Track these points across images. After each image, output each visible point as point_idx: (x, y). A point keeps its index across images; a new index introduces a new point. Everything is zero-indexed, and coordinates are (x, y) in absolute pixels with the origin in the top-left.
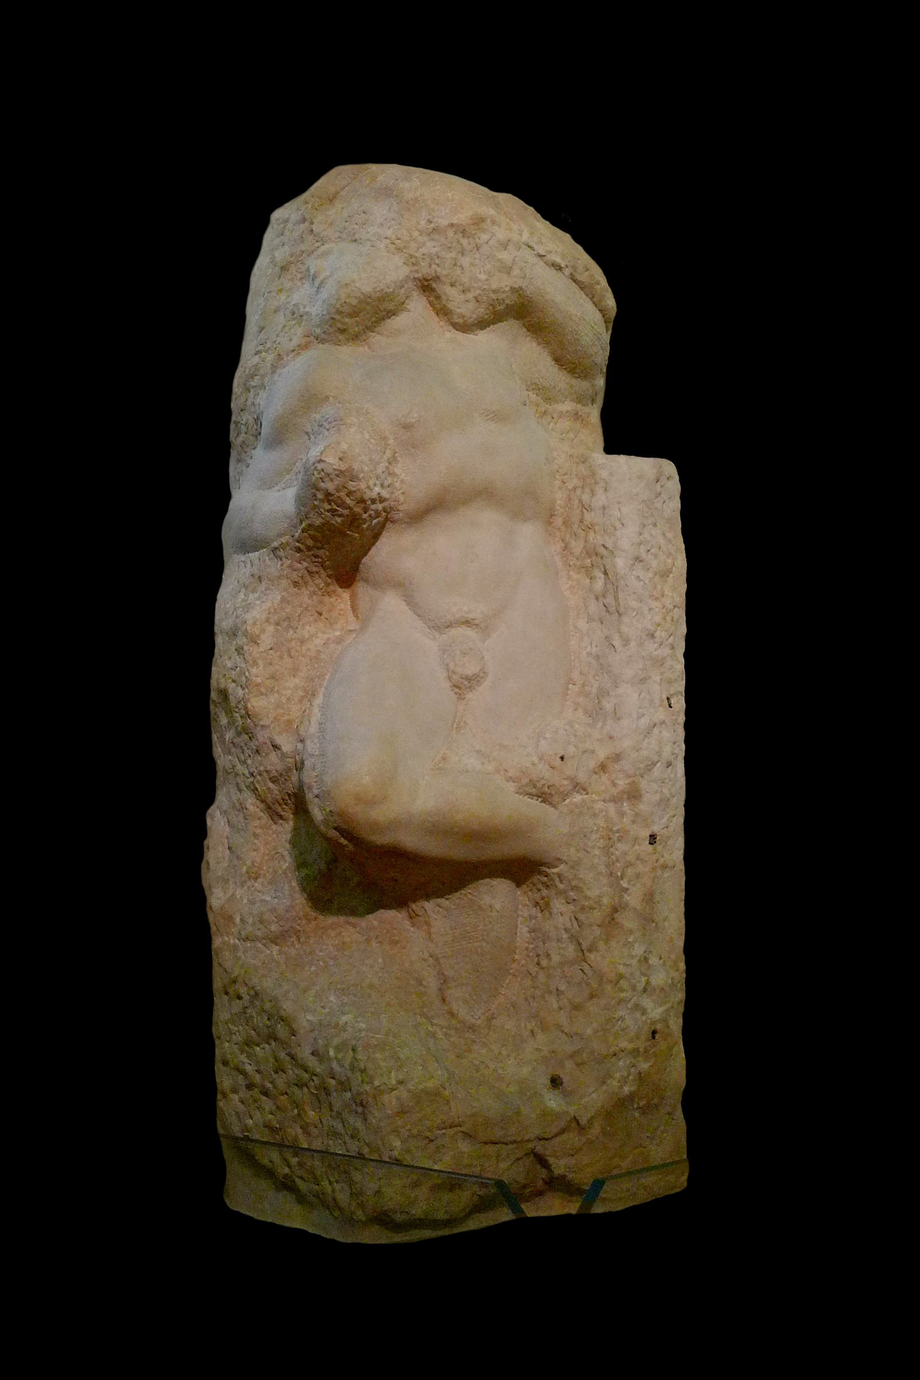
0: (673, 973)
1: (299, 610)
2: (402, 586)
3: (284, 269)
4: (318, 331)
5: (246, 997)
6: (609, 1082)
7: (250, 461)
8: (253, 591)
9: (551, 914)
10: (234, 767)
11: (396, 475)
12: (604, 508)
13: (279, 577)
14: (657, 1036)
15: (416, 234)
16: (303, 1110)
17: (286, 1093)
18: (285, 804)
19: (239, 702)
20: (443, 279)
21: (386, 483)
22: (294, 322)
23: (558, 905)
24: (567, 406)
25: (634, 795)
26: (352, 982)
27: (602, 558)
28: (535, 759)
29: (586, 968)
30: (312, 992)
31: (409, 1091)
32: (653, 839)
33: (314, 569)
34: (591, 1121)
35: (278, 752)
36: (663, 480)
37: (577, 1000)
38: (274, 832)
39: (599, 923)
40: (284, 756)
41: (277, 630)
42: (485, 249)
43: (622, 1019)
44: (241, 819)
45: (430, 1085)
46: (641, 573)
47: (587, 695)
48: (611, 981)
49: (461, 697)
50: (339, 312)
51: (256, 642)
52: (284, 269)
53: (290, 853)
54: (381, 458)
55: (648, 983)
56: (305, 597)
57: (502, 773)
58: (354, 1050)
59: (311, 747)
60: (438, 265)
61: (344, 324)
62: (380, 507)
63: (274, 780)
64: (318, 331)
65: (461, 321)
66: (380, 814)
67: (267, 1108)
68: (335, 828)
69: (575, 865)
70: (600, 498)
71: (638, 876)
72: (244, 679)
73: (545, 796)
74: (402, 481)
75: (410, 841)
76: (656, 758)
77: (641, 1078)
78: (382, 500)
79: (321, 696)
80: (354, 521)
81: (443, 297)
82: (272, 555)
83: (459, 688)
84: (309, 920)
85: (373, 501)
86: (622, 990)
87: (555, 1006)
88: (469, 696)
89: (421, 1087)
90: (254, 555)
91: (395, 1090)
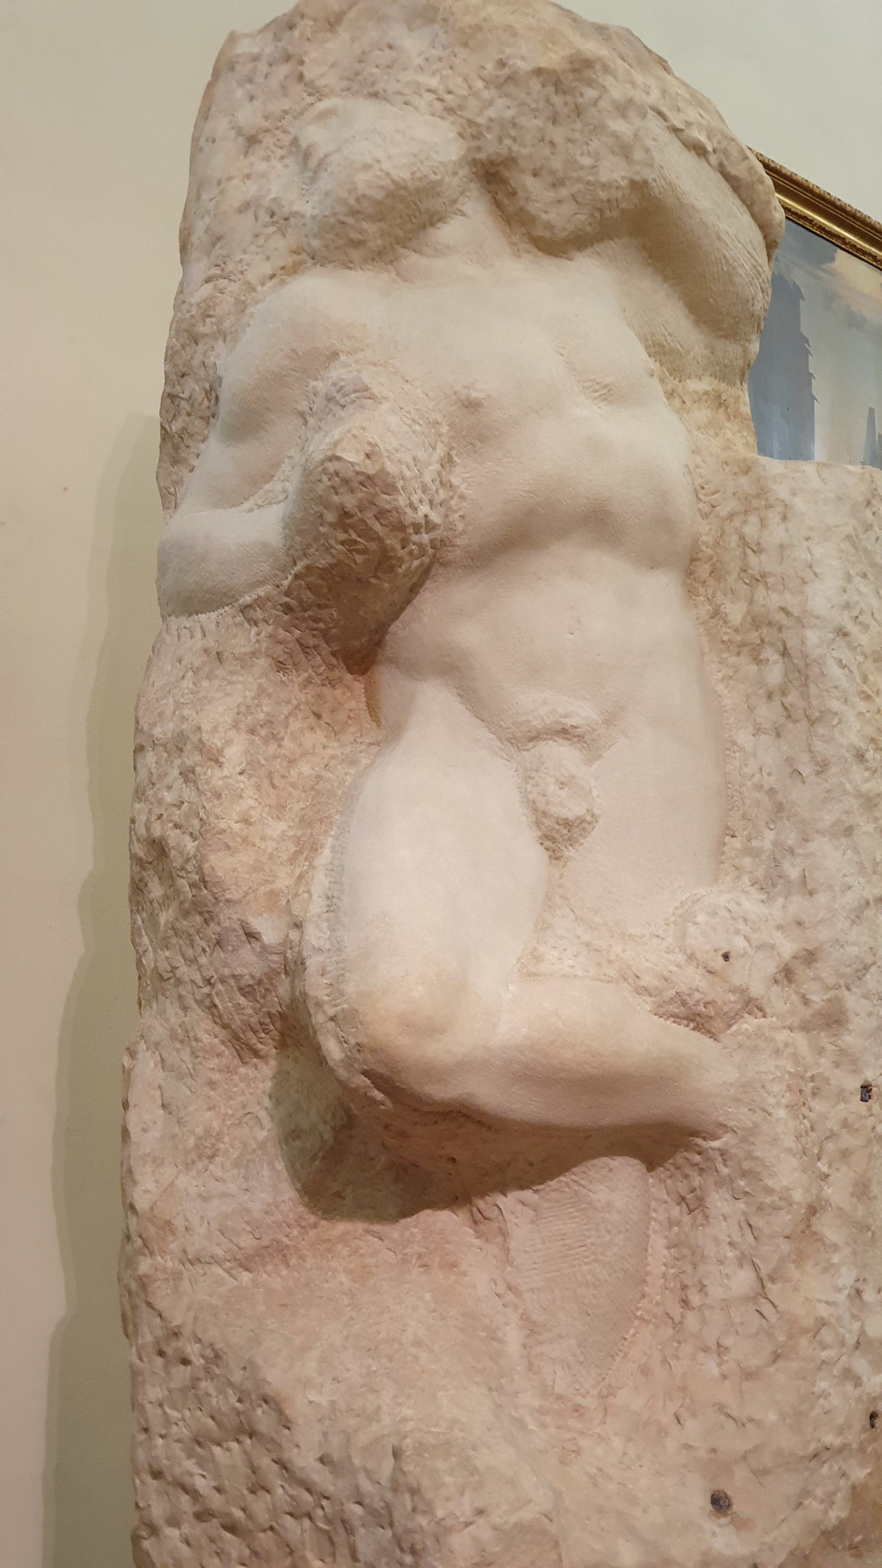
1: (286, 710)
2: (454, 669)
4: (316, 243)
5: (198, 1361)
6: (807, 1502)
7: (195, 462)
9: (706, 1217)
10: (174, 969)
11: (451, 486)
14: (878, 1422)
15: (480, 84)
16: (303, 1558)
17: (272, 1528)
18: (264, 1030)
19: (188, 860)
20: (522, 162)
21: (437, 500)
22: (272, 229)
23: (719, 1202)
24: (705, 385)
25: (833, 1019)
26: (383, 1335)
27: (780, 629)
28: (680, 958)
29: (766, 1308)
30: (315, 1354)
31: (495, 1528)
32: (866, 1091)
33: (311, 642)
35: (257, 945)
37: (754, 1362)
38: (243, 1079)
39: (787, 1232)
41: (252, 742)
43: (824, 1394)
44: (186, 1055)
45: (527, 1515)
46: (847, 656)
47: (755, 853)
48: (805, 1331)
49: (555, 856)
50: (353, 213)
51: (217, 761)
52: (252, 140)
54: (430, 456)
55: (863, 1332)
59: (315, 935)
60: (514, 140)
62: (425, 538)
63: (247, 991)
64: (316, 243)
65: (547, 234)
66: (439, 1050)
67: (234, 1554)
68: (365, 1073)
69: (749, 1135)
70: (777, 533)
71: (845, 1154)
72: (196, 822)
73: (698, 1019)
74: (462, 497)
75: (488, 1094)
76: (869, 959)
78: (430, 526)
79: (327, 852)
80: (385, 562)
81: (521, 194)
82: (240, 618)
83: (554, 840)
84: (303, 1227)
85: (417, 528)
86: (824, 1347)
88: (570, 852)
89: (514, 1519)
90: (208, 619)
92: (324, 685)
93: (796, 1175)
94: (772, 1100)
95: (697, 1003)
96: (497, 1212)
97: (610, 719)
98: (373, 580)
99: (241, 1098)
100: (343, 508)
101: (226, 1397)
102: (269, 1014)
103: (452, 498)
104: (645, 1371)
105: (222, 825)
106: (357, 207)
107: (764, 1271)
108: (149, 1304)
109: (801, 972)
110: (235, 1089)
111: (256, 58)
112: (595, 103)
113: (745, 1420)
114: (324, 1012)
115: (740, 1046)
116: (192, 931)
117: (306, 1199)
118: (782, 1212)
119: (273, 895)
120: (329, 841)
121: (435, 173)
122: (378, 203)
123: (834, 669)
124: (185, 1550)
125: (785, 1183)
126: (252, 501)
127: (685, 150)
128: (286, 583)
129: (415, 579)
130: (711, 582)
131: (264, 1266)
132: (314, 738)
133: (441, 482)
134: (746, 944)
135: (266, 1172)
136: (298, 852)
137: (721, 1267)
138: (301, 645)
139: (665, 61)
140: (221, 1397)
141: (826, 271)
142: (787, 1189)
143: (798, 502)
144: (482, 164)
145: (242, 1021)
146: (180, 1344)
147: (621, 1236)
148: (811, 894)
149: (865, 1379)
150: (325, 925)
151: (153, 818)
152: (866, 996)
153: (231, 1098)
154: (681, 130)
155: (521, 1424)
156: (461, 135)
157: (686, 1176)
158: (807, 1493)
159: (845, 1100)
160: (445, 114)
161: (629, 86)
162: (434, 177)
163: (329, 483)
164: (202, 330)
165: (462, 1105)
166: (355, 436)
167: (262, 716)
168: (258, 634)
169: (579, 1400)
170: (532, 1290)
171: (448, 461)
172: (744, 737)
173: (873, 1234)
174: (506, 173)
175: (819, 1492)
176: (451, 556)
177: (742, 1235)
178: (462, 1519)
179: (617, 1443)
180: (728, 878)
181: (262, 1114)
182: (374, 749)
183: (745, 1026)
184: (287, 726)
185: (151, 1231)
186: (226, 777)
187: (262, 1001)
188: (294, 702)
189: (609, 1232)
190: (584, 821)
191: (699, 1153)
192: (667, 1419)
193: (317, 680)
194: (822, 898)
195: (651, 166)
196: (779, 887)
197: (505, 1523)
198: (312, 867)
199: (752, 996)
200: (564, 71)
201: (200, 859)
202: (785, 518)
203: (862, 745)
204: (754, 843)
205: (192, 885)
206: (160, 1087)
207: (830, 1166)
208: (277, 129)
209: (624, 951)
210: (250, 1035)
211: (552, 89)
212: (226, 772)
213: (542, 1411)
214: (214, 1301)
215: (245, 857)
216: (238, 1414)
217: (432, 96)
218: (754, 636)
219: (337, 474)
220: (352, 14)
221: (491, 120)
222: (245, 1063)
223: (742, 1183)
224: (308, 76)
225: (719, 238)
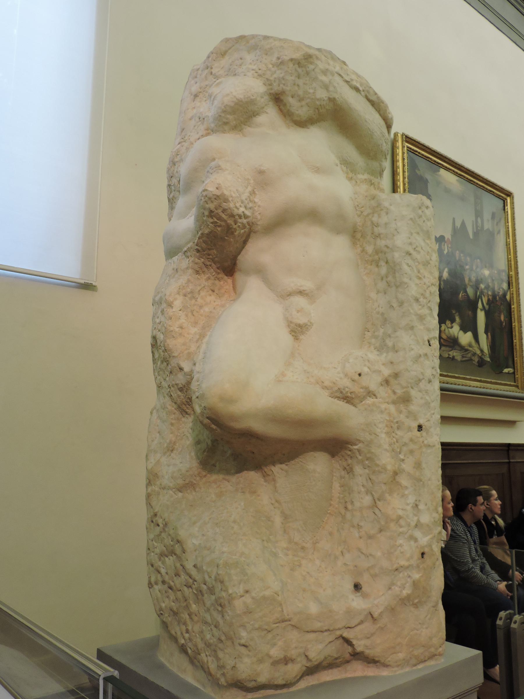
0: (435, 515)
1: (199, 288)
2: (260, 271)
3: (196, 96)
4: (213, 125)
6: (393, 588)
9: (354, 475)
12: (386, 224)
14: (425, 556)
15: (271, 66)
16: (189, 603)
17: (180, 590)
22: (200, 123)
23: (358, 469)
24: (366, 176)
25: (406, 399)
27: (385, 253)
28: (342, 375)
29: (377, 511)
31: (253, 598)
33: (208, 263)
34: (381, 614)
35: (183, 373)
36: (424, 208)
37: (372, 532)
43: (401, 545)
45: (267, 593)
46: (411, 262)
47: (376, 337)
48: (393, 520)
49: (296, 338)
52: (196, 96)
55: (418, 521)
56: (203, 280)
62: (245, 221)
66: (236, 409)
68: (207, 418)
70: (384, 219)
71: (411, 452)
73: (347, 398)
74: (259, 206)
75: (258, 426)
76: (421, 377)
77: (415, 584)
78: (246, 217)
80: (229, 230)
82: (184, 256)
84: (201, 477)
85: (240, 217)
86: (401, 527)
87: (357, 535)
88: (302, 337)
91: (243, 596)
94: (379, 430)
96: (271, 472)
98: (226, 238)
103: (255, 207)
104: (331, 534)
105: (172, 329)
107: (376, 496)
109: (392, 381)
115: (366, 409)
123: (405, 267)
124: (159, 595)
125: (384, 462)
128: (196, 241)
129: (244, 238)
130: (361, 239)
132: (211, 298)
133: (250, 200)
134: (369, 370)
138: (205, 265)
143: (392, 208)
148: (397, 352)
149: (419, 539)
152: (420, 391)
155: (275, 555)
156: (264, 84)
158: (393, 584)
159: (411, 431)
162: (252, 97)
164: (176, 160)
167: (189, 290)
169: (304, 544)
171: (253, 193)
172: (373, 295)
173: (423, 483)
174: (282, 98)
175: (399, 583)
178: (239, 594)
179: (318, 562)
181: (189, 435)
183: (368, 402)
188: (203, 285)
190: (307, 325)
191: (350, 451)
193: (213, 278)
198: (202, 343)
201: (165, 341)
202: (387, 213)
203: (418, 296)
204: (376, 334)
205: (163, 351)
210: (184, 406)
211: (297, 66)
212: (174, 310)
213: (287, 549)
215: (180, 340)
218: (376, 257)
221: (275, 78)
223: (367, 462)
225: (366, 121)
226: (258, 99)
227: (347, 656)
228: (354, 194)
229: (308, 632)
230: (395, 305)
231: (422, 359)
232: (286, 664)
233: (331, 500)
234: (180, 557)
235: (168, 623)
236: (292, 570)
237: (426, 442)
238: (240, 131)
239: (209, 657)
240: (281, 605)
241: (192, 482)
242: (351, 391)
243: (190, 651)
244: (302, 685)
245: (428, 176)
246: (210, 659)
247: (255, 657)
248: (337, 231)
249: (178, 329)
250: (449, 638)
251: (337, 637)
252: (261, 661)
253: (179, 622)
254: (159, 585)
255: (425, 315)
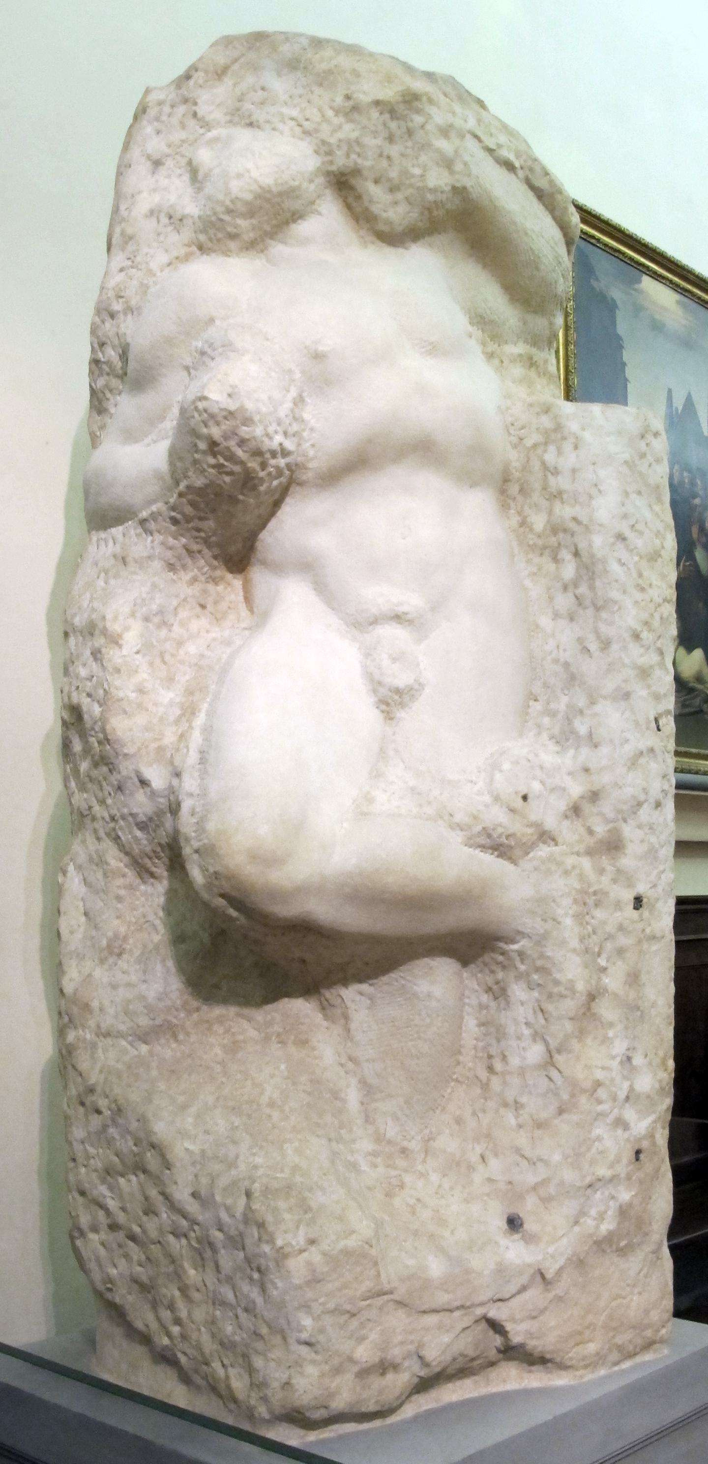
1: (175, 602)
2: (308, 567)
6: (582, 1221)
8: (116, 577)
9: (508, 1003)
10: (90, 808)
11: (303, 421)
12: (574, 471)
13: (150, 558)
14: (642, 1156)
15: (330, 113)
17: (159, 1242)
18: (156, 857)
19: (95, 723)
20: (365, 173)
23: (518, 991)
24: (520, 348)
25: (613, 845)
26: (246, 1097)
27: (572, 535)
28: (487, 799)
29: (554, 1074)
30: (192, 1110)
31: (324, 1254)
32: (638, 902)
33: (195, 547)
35: (148, 790)
36: (649, 437)
37: (543, 1115)
38: (145, 894)
39: (571, 1014)
40: (153, 794)
42: (420, 135)
43: (599, 1139)
44: (100, 875)
45: (351, 1242)
46: (624, 555)
47: (553, 714)
48: (584, 1091)
49: (389, 716)
50: (229, 211)
51: (117, 643)
52: (157, 163)
53: (164, 924)
55: (631, 1089)
57: (446, 818)
58: (248, 1194)
59: (189, 784)
60: (359, 155)
61: (236, 226)
62: (282, 462)
63: (142, 826)
65: (386, 229)
66: (284, 877)
68: (223, 896)
69: (542, 939)
70: (570, 459)
71: (620, 952)
72: (101, 692)
73: (501, 847)
75: (323, 911)
76: (642, 797)
78: (285, 453)
80: (248, 481)
81: (365, 197)
82: (140, 530)
83: (388, 704)
85: (274, 454)
86: (600, 1102)
88: (401, 714)
90: (117, 531)
91: (304, 1251)
92: (207, 582)
93: (579, 970)
95: (500, 836)
96: (340, 1000)
97: (434, 608)
98: (241, 497)
99: (141, 910)
100: (211, 438)
101: (126, 1141)
102: (160, 844)
103: (304, 430)
104: (459, 1121)
105: (121, 694)
106: (232, 207)
107: (553, 1044)
108: (74, 1067)
109: (587, 808)
110: (137, 903)
111: (160, 103)
112: (422, 127)
113: (535, 1160)
114: (191, 846)
115: (536, 869)
116: (101, 778)
117: (190, 989)
118: (569, 1000)
119: (160, 750)
120: (205, 706)
121: (294, 180)
122: (246, 203)
123: (614, 567)
124: (102, 1252)
125: (570, 976)
126: (150, 437)
127: (498, 166)
128: (172, 500)
129: (276, 496)
130: (520, 498)
131: (158, 1040)
133: (294, 417)
135: (159, 967)
136: (183, 715)
137: (519, 1042)
138: (187, 550)
139: (482, 101)
140: (123, 1141)
141: (635, 290)
142: (571, 981)
143: (587, 436)
144: (334, 175)
145: (140, 850)
146: (94, 1098)
147: (440, 1019)
148: (596, 746)
149: (632, 1125)
150: (196, 774)
151: (73, 688)
152: (640, 827)
153: (135, 909)
154: (494, 150)
155: (354, 1167)
157: (492, 972)
158: (582, 1213)
159: (621, 910)
160: (303, 136)
161: (450, 115)
163: (199, 419)
165: (304, 921)
166: (219, 381)
167: (154, 607)
168: (152, 542)
169: (405, 1144)
170: (368, 1060)
171: (299, 401)
172: (545, 621)
173: (642, 1012)
174: (353, 181)
176: (304, 477)
177: (536, 1018)
178: (297, 1248)
179: (434, 1178)
180: (532, 734)
181: (158, 922)
182: (247, 633)
183: (540, 853)
184: (176, 615)
185: (75, 1010)
186: (124, 656)
187: (153, 835)
188: (182, 596)
189: (428, 1016)
190: (412, 689)
191: (502, 954)
192: (475, 1158)
193: (203, 578)
194: (604, 750)
195: (469, 175)
196: (571, 741)
197: (333, 1250)
198: (191, 727)
199: (546, 829)
200: (398, 103)
201: (103, 720)
202: (576, 447)
204: (553, 706)
205: (99, 743)
206: (83, 899)
207: (608, 961)
208: (177, 154)
209: (441, 794)
210: (147, 861)
211: (387, 116)
213: (374, 1154)
214: (120, 1066)
215: (140, 720)
216: (135, 1155)
217: (293, 123)
218: (553, 541)
219: (206, 411)
220: (236, 67)
221: (340, 141)
222: (144, 882)
224: (200, 114)
225: (526, 234)
226: (305, 185)
227: (493, 1354)
228: (505, 397)
229: (424, 1312)
230: (593, 647)
231: (642, 760)
232: (383, 1374)
233: (460, 1053)
234: (158, 1177)
235: (127, 1307)
236: (389, 1195)
237: (648, 931)
238: (262, 251)
239: (230, 1369)
240: (376, 1264)
241: (169, 1022)
242: (510, 832)
243: (183, 1359)
244: (408, 1411)
245: (616, 293)
246: (232, 1372)
247: (326, 1363)
248: (469, 479)
249: (134, 695)
250: (679, 1313)
251: (477, 1318)
252: (338, 1371)
253: (155, 1305)
254: (102, 1233)
255: (651, 667)
